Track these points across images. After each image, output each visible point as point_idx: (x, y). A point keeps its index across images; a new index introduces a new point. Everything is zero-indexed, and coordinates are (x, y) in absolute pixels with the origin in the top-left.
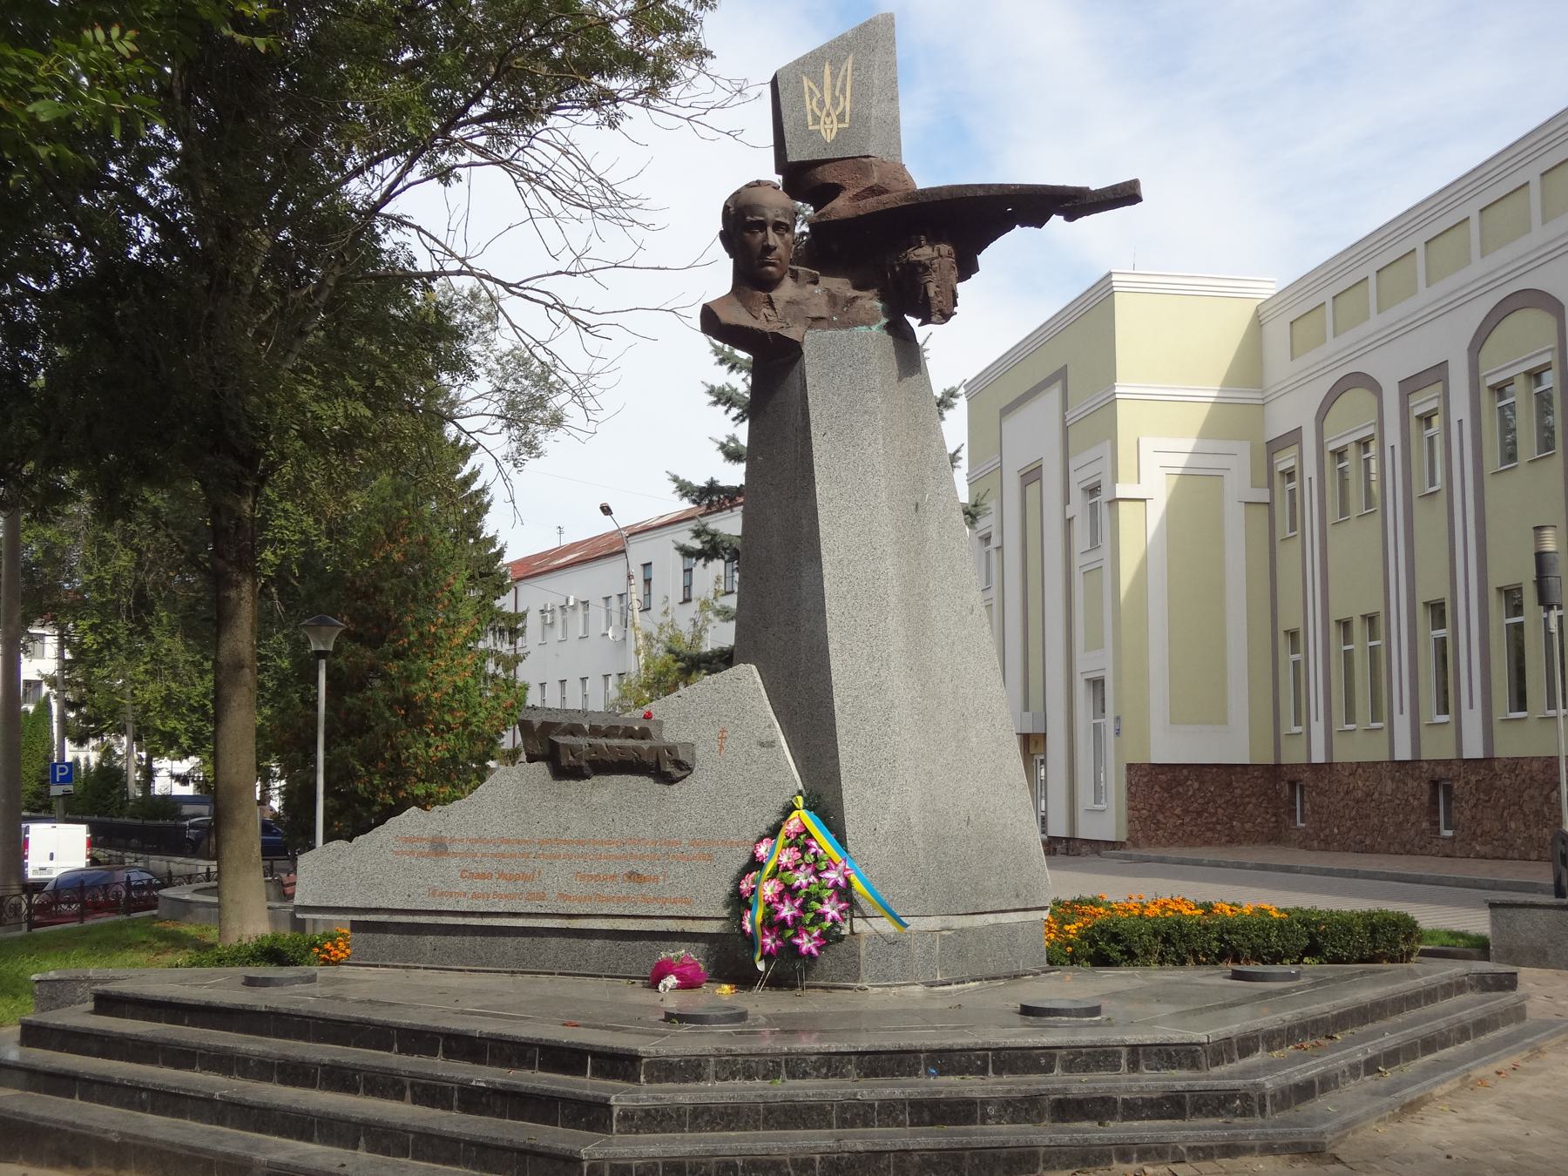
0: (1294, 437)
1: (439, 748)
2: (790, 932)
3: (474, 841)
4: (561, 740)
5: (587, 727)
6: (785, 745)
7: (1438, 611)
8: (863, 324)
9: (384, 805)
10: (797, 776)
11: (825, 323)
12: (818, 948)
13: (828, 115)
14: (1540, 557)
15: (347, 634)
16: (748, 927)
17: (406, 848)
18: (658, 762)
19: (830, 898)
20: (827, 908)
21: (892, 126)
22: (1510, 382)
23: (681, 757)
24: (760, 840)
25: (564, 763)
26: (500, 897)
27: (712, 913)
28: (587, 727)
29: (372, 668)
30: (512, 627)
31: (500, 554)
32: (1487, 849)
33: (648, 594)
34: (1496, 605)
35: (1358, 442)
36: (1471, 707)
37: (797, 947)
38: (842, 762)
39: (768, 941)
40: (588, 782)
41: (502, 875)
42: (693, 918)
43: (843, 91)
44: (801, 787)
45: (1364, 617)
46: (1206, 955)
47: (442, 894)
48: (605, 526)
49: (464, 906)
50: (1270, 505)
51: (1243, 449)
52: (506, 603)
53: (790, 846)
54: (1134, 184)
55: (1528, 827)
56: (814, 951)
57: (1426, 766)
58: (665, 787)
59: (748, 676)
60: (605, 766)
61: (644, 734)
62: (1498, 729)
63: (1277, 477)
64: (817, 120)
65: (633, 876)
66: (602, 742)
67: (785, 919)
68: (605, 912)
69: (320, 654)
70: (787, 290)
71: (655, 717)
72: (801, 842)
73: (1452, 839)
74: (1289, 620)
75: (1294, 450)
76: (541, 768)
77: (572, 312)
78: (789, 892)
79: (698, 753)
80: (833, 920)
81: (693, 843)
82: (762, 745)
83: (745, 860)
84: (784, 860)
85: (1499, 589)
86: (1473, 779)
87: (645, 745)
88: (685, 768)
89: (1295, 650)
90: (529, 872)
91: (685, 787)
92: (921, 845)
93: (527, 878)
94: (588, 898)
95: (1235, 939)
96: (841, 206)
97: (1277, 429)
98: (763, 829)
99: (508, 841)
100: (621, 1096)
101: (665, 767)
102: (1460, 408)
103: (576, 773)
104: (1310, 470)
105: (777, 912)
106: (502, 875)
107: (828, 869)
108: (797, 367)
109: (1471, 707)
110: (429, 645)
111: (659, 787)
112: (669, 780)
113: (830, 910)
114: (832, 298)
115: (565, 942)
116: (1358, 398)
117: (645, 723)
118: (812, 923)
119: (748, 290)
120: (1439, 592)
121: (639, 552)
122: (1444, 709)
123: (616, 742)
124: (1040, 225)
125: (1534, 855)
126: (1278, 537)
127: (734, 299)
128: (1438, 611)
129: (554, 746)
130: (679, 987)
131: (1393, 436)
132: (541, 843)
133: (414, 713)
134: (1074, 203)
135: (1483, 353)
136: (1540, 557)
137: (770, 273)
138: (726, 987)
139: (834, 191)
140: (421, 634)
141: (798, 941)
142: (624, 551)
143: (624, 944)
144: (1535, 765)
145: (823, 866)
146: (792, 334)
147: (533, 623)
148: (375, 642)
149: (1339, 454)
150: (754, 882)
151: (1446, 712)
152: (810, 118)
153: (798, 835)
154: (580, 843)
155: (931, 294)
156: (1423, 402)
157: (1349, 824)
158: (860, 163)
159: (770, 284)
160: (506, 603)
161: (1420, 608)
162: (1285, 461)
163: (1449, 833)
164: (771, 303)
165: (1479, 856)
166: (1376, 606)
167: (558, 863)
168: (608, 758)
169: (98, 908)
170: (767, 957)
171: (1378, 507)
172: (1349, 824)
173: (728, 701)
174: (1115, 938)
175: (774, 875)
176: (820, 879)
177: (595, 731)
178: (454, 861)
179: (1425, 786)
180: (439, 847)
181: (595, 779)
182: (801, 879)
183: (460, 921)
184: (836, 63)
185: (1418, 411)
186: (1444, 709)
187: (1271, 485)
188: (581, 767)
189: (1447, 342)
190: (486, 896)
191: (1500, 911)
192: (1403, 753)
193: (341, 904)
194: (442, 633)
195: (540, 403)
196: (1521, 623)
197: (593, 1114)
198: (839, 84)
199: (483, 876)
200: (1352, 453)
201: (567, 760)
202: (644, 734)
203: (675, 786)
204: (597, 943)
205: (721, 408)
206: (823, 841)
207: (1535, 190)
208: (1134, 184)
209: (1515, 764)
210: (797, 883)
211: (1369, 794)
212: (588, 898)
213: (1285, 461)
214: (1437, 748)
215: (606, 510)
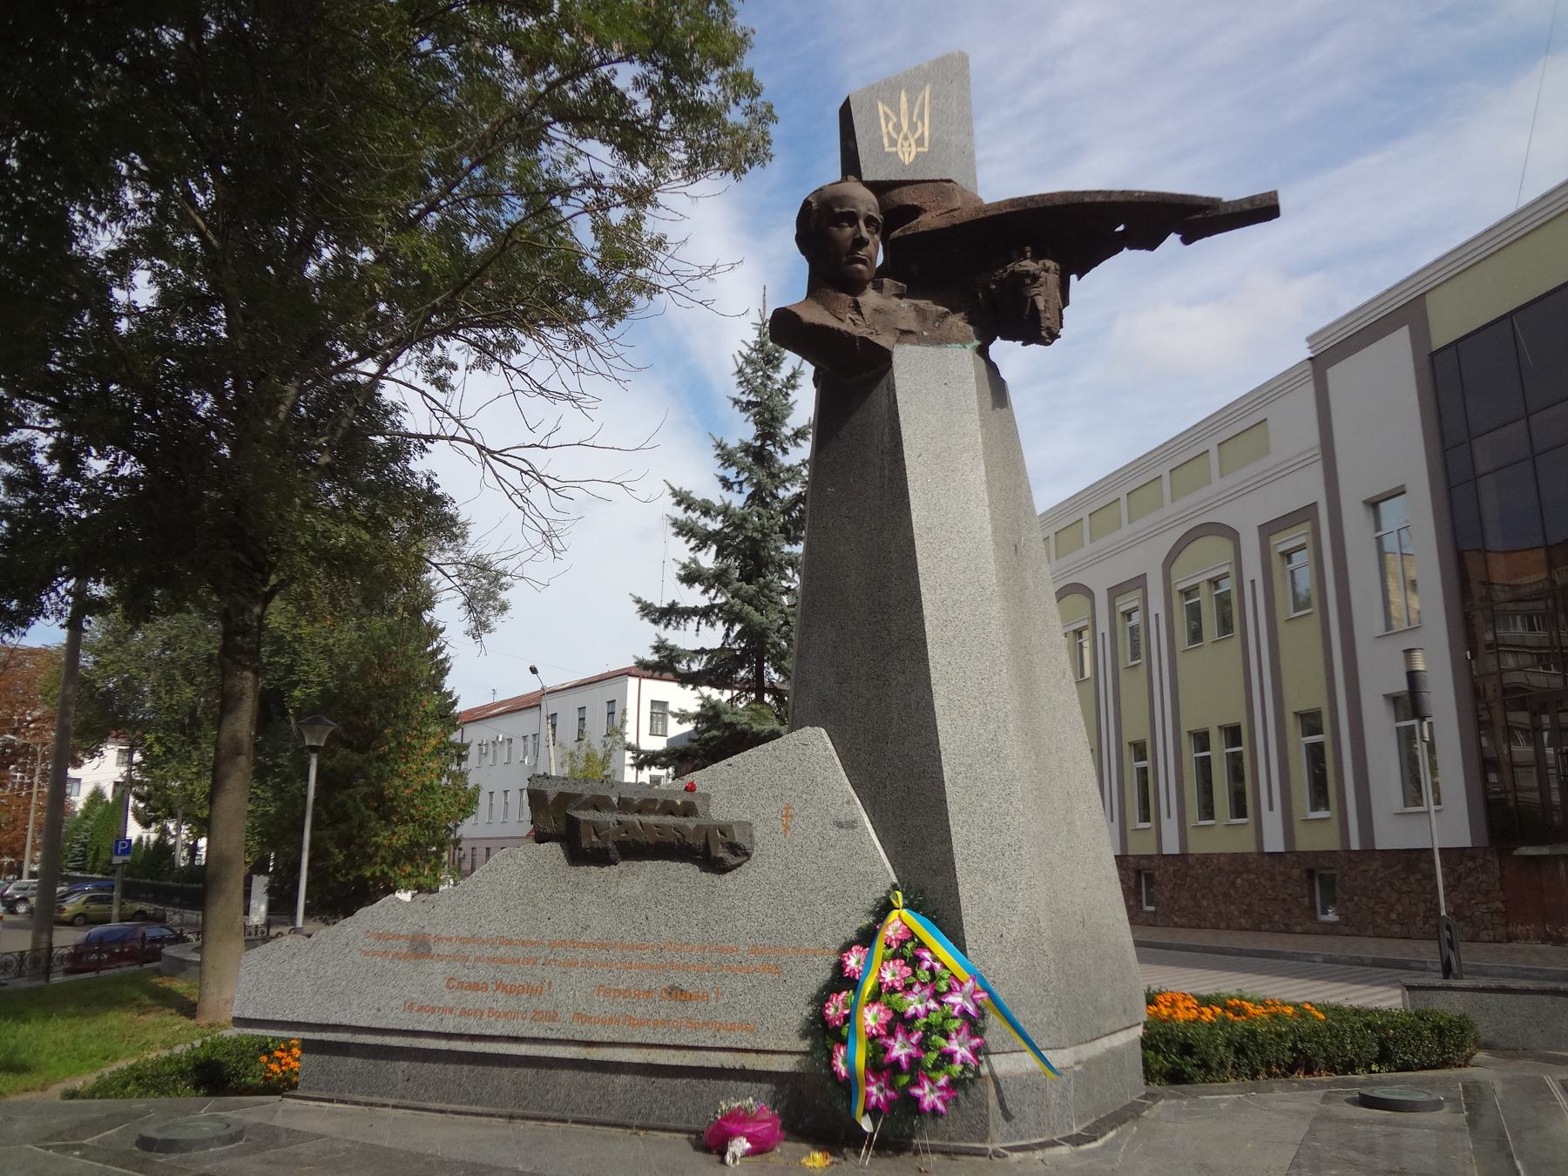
1: (402, 836)
2: (905, 1080)
3: (464, 941)
4: (582, 815)
5: (615, 800)
6: (869, 825)
8: (957, 341)
9: (604, 88)
10: (888, 865)
11: (910, 337)
12: (945, 1102)
13: (906, 138)
14: (1412, 676)
15: (333, 738)
16: (841, 1068)
17: (378, 947)
18: (707, 845)
19: (958, 1032)
20: (953, 1046)
21: (967, 155)
22: (1196, 588)
23: (738, 839)
24: (847, 948)
25: (585, 844)
26: (497, 1015)
27: (785, 1046)
28: (615, 800)
29: (359, 769)
30: (460, 752)
31: (455, 703)
32: (1184, 921)
34: (1188, 745)
36: (1271, 809)
37: (918, 1100)
38: (956, 848)
39: (874, 1089)
40: (615, 869)
41: (500, 986)
42: (758, 1052)
43: (921, 116)
44: (895, 880)
46: (1279, 1066)
47: (421, 1009)
48: (531, 685)
49: (449, 1026)
52: (455, 737)
53: (894, 957)
54: (1273, 195)
56: (940, 1106)
58: (715, 877)
59: (814, 747)
60: (636, 849)
61: (688, 810)
62: (1190, 832)
64: (893, 143)
65: (675, 992)
66: (635, 818)
67: (898, 1060)
68: (637, 1039)
69: (314, 749)
71: (699, 789)
72: (909, 952)
73: (1154, 913)
76: (554, 850)
77: (546, 480)
78: (900, 1022)
79: (757, 834)
80: (964, 1063)
81: (754, 950)
82: (840, 825)
83: (826, 974)
84: (888, 977)
85: (1296, 714)
87: (690, 823)
88: (741, 852)
90: (536, 983)
91: (741, 878)
92: (1051, 955)
93: (533, 991)
94: (613, 1020)
95: (1309, 1048)
98: (851, 934)
99: (510, 942)
101: (714, 852)
102: (1157, 605)
103: (600, 858)
105: (886, 1050)
106: (500, 986)
107: (951, 990)
108: (884, 382)
109: (1271, 809)
110: (405, 751)
111: (707, 877)
112: (719, 867)
113: (959, 1048)
115: (580, 1076)
117: (688, 797)
118: (937, 1067)
119: (831, 292)
121: (550, 705)
122: (1145, 817)
123: (652, 819)
124: (1152, 247)
125: (1222, 925)
127: (812, 303)
128: (1139, 750)
129: (573, 823)
130: (748, 1153)
131: (1103, 626)
132: (552, 945)
133: (385, 809)
134: (1195, 218)
136: (1412, 676)
137: (860, 271)
138: (818, 1156)
140: (399, 744)
141: (918, 1092)
143: (660, 1082)
145: (943, 986)
146: (883, 340)
147: (473, 751)
148: (361, 749)
150: (845, 1005)
152: (886, 141)
153: (902, 943)
154: (603, 946)
155: (1041, 306)
156: (1124, 604)
158: (943, 186)
159: (853, 286)
160: (455, 737)
161: (1185, 736)
163: (1152, 908)
164: (857, 308)
165: (1176, 925)
166: (1237, 716)
167: (575, 972)
168: (641, 839)
169: (121, 957)
170: (873, 1112)
171: (1142, 660)
173: (792, 772)
174: (1187, 1049)
175: (875, 998)
176: (941, 1003)
177: (625, 805)
178: (439, 966)
179: (1132, 874)
180: (420, 947)
181: (622, 865)
182: (914, 1004)
183: (443, 1045)
184: (913, 92)
186: (1146, 818)
188: (606, 851)
189: (1148, 559)
190: (479, 1013)
191: (1417, 993)
193: (290, 1018)
194: (415, 742)
195: (490, 596)
198: (916, 111)
199: (475, 987)
200: (1204, 589)
201: (589, 840)
202: (688, 810)
203: (728, 876)
204: (624, 1079)
205: (682, 539)
206: (939, 948)
208: (1273, 195)
209: (1205, 858)
210: (911, 1011)
212: (613, 1020)
215: (534, 670)
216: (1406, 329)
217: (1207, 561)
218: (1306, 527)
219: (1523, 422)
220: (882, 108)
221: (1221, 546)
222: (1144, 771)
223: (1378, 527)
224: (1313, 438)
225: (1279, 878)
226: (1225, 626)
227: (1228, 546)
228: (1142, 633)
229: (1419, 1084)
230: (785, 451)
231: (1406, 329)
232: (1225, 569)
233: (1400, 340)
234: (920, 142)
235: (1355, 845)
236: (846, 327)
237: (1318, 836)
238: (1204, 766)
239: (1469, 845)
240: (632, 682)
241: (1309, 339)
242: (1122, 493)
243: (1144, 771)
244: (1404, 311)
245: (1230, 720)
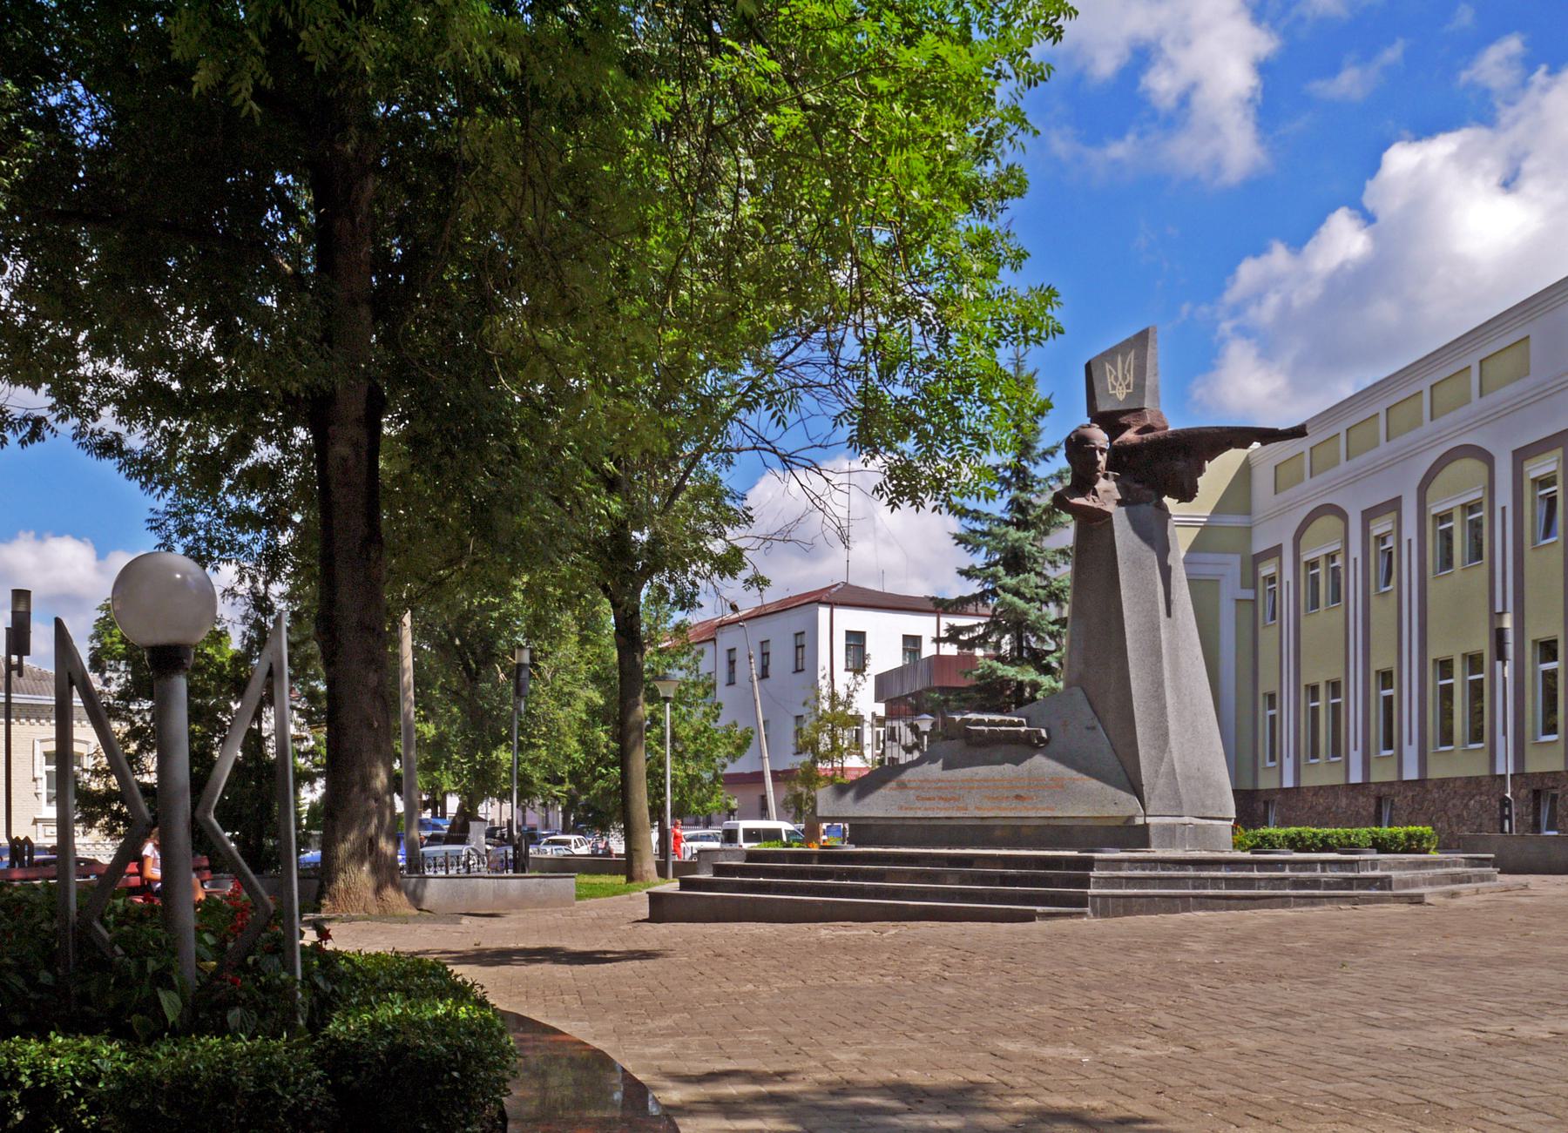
0: (1276, 551)
33: (732, 672)
35: (1327, 555)
64: (1114, 388)
65: (1018, 797)
89: (1272, 706)
96: (1130, 436)
97: (1259, 546)
102: (1410, 530)
116: (1328, 523)
122: (1272, 759)
128: (1386, 678)
130: (1132, 818)
142: (714, 640)
144: (1458, 783)
151: (1390, 748)
156: (1380, 527)
162: (1267, 569)
166: (1337, 674)
179: (1373, 801)
184: (1125, 356)
185: (1376, 532)
200: (1322, 564)
209: (1443, 783)
211: (1328, 808)
213: (1267, 569)
220: (1108, 366)
221: (1469, 467)
222: (1336, 707)
226: (1476, 553)
229: (1402, 866)
230: (1036, 463)
234: (1128, 387)
236: (1090, 504)
238: (1447, 692)
240: (824, 612)
242: (1380, 408)
245: (1333, 677)
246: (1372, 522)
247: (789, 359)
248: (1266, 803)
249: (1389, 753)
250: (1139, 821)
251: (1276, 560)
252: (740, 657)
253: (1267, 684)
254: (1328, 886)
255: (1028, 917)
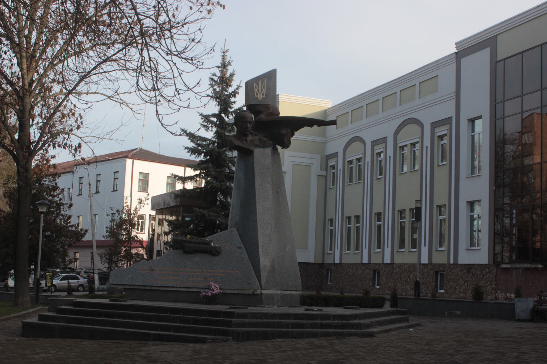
0: (335, 155)
7: (379, 216)
22: (406, 146)
35: (357, 159)
36: (388, 247)
45: (355, 216)
50: (326, 177)
51: (319, 157)
55: (403, 285)
57: (372, 265)
63: (329, 168)
64: (257, 94)
70: (250, 138)
73: (379, 289)
74: (329, 216)
75: (335, 159)
85: (375, 213)
86: (387, 270)
89: (331, 225)
96: (263, 116)
97: (329, 151)
100: (234, 320)
102: (390, 152)
104: (340, 166)
109: (388, 247)
112: (214, 255)
114: (260, 139)
116: (357, 145)
120: (380, 210)
122: (331, 250)
123: (200, 246)
126: (328, 188)
128: (379, 216)
131: (427, 143)
135: (398, 136)
139: (261, 112)
144: (406, 266)
146: (251, 149)
149: (351, 162)
156: (440, 131)
157: (346, 283)
158: (267, 107)
159: (246, 136)
161: (373, 215)
162: (332, 163)
163: (378, 287)
164: (246, 141)
166: (360, 213)
171: (362, 181)
172: (346, 283)
179: (372, 272)
185: (377, 151)
187: (326, 170)
189: (387, 130)
192: (365, 261)
196: (401, 219)
197: (229, 324)
200: (354, 162)
207: (417, 87)
209: (400, 265)
213: (332, 163)
214: (376, 260)
216: (489, 49)
217: (410, 135)
218: (447, 127)
219: (520, 98)
223: (473, 131)
224: (453, 89)
225: (426, 274)
227: (419, 129)
228: (383, 164)
231: (489, 49)
232: (417, 140)
233: (486, 53)
234: (263, 94)
235: (452, 262)
237: (439, 259)
239: (487, 263)
241: (456, 44)
242: (417, 82)
243: (379, 227)
244: (486, 42)
246: (375, 147)
247: (114, 57)
248: (328, 270)
249: (379, 250)
250: (259, 292)
251: (336, 159)
252: (85, 181)
253: (329, 216)
254: (336, 327)
255: (203, 341)
